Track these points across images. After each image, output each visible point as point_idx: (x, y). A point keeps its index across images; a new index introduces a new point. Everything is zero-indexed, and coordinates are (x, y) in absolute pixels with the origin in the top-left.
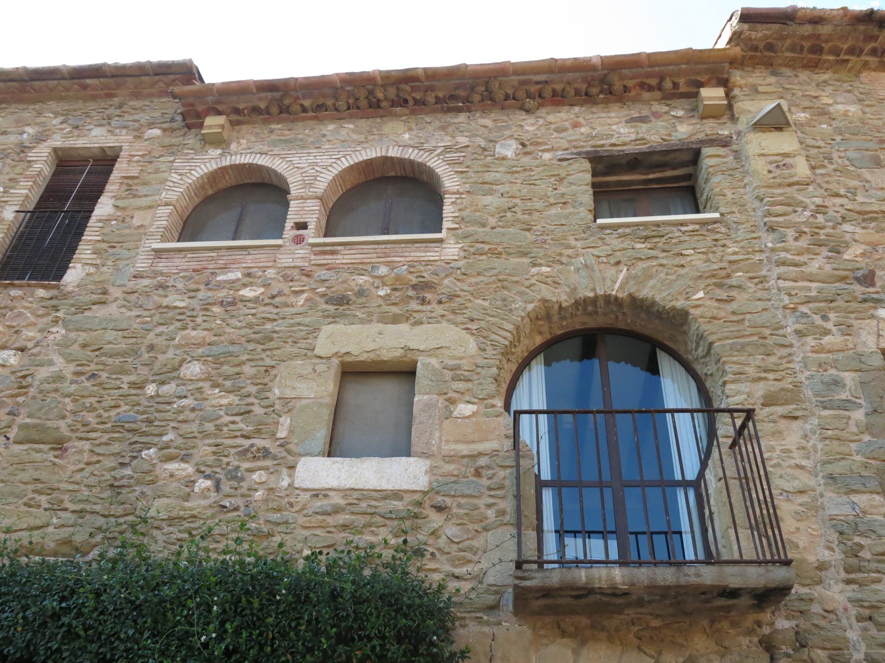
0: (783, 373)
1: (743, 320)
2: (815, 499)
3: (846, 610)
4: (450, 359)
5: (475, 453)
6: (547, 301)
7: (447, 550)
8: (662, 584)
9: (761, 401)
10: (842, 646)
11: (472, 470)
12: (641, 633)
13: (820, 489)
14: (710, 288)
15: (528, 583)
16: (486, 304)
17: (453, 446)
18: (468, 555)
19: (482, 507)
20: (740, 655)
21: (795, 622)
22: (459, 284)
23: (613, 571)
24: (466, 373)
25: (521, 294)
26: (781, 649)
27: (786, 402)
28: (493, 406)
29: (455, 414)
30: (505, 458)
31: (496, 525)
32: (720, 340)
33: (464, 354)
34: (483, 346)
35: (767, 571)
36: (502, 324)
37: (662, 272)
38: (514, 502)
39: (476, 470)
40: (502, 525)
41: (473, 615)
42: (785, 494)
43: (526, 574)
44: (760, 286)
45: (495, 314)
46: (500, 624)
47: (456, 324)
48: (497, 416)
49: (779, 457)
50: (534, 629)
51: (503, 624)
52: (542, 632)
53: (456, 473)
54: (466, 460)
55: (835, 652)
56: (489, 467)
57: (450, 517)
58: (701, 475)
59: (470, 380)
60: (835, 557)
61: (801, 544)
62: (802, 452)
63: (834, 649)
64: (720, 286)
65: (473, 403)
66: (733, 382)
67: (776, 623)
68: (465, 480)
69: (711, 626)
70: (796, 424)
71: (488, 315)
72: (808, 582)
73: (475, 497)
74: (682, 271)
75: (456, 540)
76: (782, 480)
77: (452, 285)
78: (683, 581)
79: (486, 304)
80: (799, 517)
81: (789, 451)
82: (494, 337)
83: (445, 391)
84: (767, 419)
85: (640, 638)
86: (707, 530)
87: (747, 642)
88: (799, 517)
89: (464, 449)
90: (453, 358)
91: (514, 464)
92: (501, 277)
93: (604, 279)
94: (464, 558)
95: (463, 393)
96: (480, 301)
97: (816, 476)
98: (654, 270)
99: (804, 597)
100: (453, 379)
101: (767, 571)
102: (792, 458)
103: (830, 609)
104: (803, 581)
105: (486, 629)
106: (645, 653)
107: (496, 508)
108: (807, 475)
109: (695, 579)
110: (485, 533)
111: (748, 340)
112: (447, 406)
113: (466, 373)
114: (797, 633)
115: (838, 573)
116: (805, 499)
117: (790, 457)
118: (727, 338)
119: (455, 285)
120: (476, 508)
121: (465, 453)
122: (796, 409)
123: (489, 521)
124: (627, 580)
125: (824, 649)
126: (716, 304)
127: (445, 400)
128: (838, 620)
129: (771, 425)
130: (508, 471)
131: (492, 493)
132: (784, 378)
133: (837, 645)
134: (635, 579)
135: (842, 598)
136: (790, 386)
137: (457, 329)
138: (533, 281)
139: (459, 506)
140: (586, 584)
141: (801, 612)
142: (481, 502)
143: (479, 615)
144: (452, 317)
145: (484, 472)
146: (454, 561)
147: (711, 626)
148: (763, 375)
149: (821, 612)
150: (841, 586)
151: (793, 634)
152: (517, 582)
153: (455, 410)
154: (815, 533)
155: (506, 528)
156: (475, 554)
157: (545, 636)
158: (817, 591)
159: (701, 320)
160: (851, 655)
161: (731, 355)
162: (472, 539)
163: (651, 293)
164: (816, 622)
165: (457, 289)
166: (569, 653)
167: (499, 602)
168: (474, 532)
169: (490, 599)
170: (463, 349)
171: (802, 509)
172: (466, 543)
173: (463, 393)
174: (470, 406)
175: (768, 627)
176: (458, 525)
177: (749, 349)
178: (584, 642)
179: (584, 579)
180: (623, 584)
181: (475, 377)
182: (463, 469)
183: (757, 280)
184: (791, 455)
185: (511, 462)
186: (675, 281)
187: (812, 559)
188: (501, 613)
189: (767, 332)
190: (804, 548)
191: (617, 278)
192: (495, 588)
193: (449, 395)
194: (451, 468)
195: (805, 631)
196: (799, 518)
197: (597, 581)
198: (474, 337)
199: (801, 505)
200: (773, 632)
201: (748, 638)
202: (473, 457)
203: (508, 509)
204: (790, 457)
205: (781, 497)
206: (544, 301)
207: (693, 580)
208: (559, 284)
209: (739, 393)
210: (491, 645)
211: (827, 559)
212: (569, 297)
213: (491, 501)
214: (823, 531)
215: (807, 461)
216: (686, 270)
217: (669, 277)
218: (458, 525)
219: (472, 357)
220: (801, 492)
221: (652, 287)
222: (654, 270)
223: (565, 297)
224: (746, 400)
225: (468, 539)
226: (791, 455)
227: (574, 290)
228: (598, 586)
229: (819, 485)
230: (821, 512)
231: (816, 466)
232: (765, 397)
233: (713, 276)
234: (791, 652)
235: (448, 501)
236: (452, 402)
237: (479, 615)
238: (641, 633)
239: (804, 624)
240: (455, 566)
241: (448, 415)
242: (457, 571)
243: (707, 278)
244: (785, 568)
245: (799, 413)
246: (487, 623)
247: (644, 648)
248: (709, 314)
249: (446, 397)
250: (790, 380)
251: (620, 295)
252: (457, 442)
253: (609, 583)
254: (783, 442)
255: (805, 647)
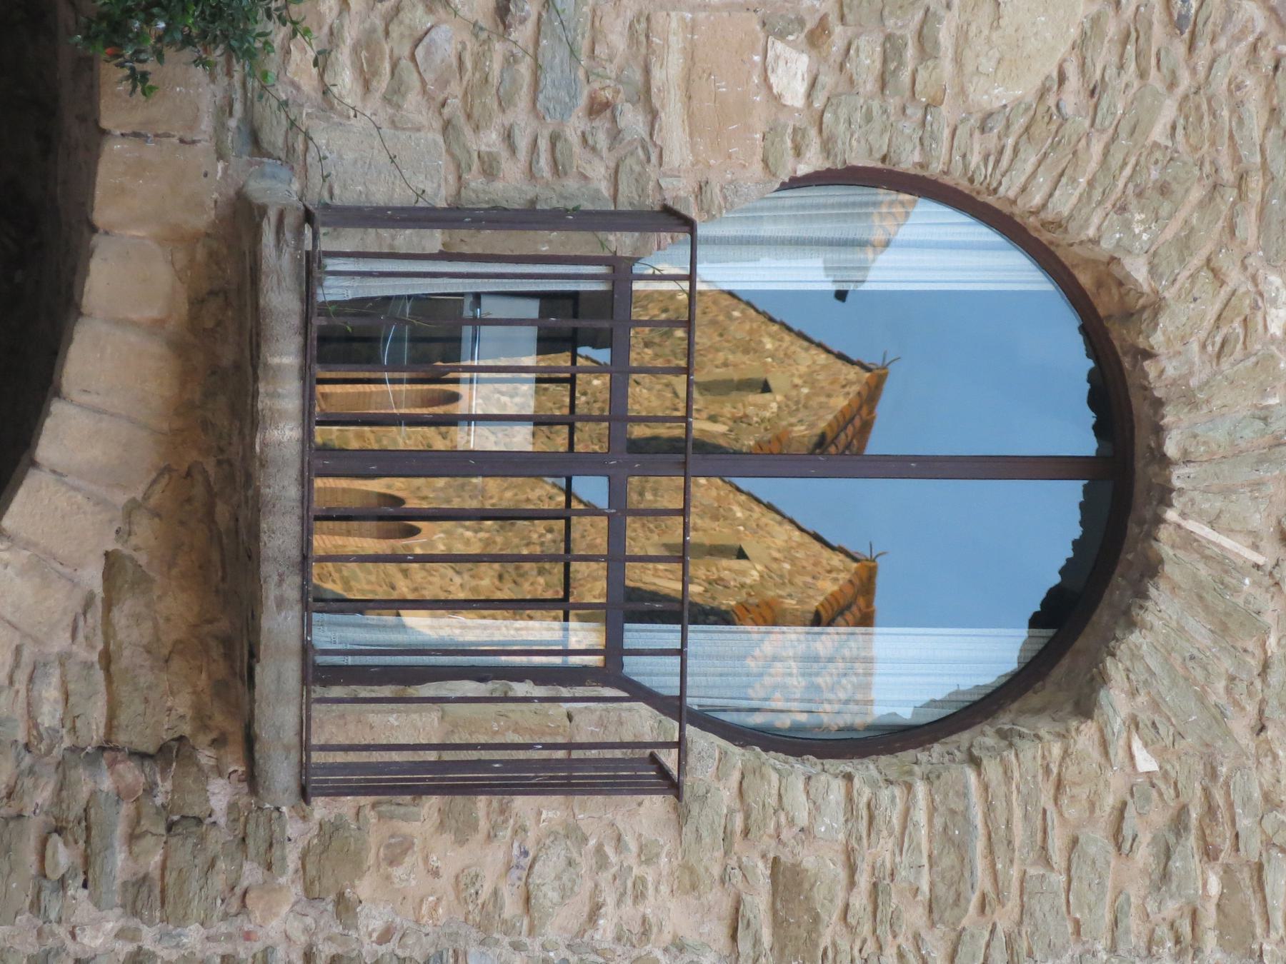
0: (866, 929)
1: (1047, 862)
2: (508, 928)
3: (248, 936)
4: (959, 28)
5: (656, 102)
6: (1156, 315)
7: (395, 30)
8: (264, 526)
9: (786, 858)
10: (169, 909)
11: (608, 94)
12: (199, 478)
13: (535, 945)
14: (1169, 793)
15: (268, 237)
16: (1158, 133)
17: (676, 42)
18: (383, 83)
19: (508, 119)
20: (149, 688)
21: (222, 821)
22: (1242, 48)
23: (292, 424)
24: (905, 76)
25: (1185, 244)
26: (164, 780)
27: (778, 923)
28: (798, 152)
29: (778, 47)
30: (640, 179)
31: (457, 152)
32: (986, 788)
33: (969, 68)
34: (998, 125)
35: (287, 749)
36: (1074, 180)
37: (1241, 664)
38: (517, 203)
39: (607, 105)
40: (459, 166)
41: (238, 95)
42: (526, 862)
43: (289, 236)
44: (1163, 931)
45: (1115, 161)
46: (221, 156)
47: (1082, 44)
48: (765, 161)
49: (624, 871)
50: (208, 235)
51: (220, 166)
52: (201, 254)
53: (601, 51)
54: (638, 76)
55: (157, 891)
56: (615, 135)
57: (484, 35)
58: (639, 693)
59: (883, 87)
60: (366, 940)
61: (398, 872)
62: (637, 928)
63: (163, 891)
64: (1179, 823)
65: (809, 95)
66: (850, 799)
67: (221, 782)
68: (581, 74)
69: (216, 637)
70: (719, 932)
71: (1114, 138)
72: (312, 871)
73: (534, 101)
74: (1240, 727)
75: (420, 52)
76: (562, 863)
77: (1233, 29)
78: (269, 570)
79: (1158, 133)
80: (465, 883)
81: (639, 897)
82: (1029, 160)
83: (850, 18)
84: (733, 862)
85: (189, 474)
86: (482, 680)
87: (181, 711)
88: (465, 883)
89: (668, 72)
90: (962, 37)
91: (624, 206)
92: (1255, 183)
93: (1226, 492)
94: (375, 73)
95: (842, 67)
96: (1169, 110)
97: (569, 946)
98: (1251, 645)
99: (276, 852)
100: (889, 38)
101: (287, 749)
102: (619, 902)
103: (248, 901)
104: (311, 859)
105: (206, 124)
106: (154, 482)
107: (504, 154)
108: (575, 926)
109: (272, 597)
110: (437, 125)
111: (980, 864)
112: (801, 22)
113: (905, 76)
114: (199, 821)
115: (329, 939)
116: (511, 907)
117: (623, 894)
118: (989, 808)
119: (1237, 39)
120: (504, 103)
121: (658, 75)
122: (757, 942)
123: (467, 131)
124: (272, 453)
125: (163, 868)
126: (1109, 802)
127: (823, 20)
128: (226, 916)
129: (716, 871)
130: (605, 188)
131: (543, 144)
132: (852, 930)
133: (170, 899)
134: (272, 470)
135: (272, 934)
136: (825, 941)
137: (1063, 49)
138: (1235, 277)
139: (511, 60)
140: (266, 364)
141: (244, 839)
142: (520, 115)
143: (238, 107)
144: (1112, 29)
145: (602, 124)
146: (368, 48)
147: (216, 637)
148: (864, 880)
149: (245, 884)
150: (302, 939)
151: (196, 811)
152: (273, 214)
153: (793, 45)
154: (425, 908)
155: (452, 179)
156: (387, 100)
157: (192, 260)
158: (289, 884)
159: (1056, 749)
160: (150, 923)
161: (933, 809)
162: (424, 91)
163: (1158, 624)
164: (221, 865)
165: (1222, 43)
166: (153, 313)
167: (270, 156)
168: (441, 98)
169: (275, 135)
170: (988, 66)
171: (485, 894)
172: (414, 79)
173: (842, 67)
174: (801, 88)
175: (212, 762)
176: (460, 58)
177: (949, 860)
178: (180, 349)
179: (275, 361)
180: (265, 445)
181: (893, 103)
182: (611, 70)
183: (1186, 928)
184: (629, 901)
185: (628, 198)
186: (1201, 699)
187: (364, 888)
188: (245, 158)
189: (1005, 918)
190: (388, 878)
191: (1229, 532)
192: (300, 147)
193: (838, 29)
194: (617, 39)
195: (202, 839)
196: (463, 880)
197: (271, 388)
198: (1031, 98)
199: (495, 893)
200: (200, 769)
201: (189, 714)
202: (645, 97)
203: (499, 185)
204: (623, 894)
205: (516, 851)
206: (1156, 306)
207: (271, 592)
208: (1219, 355)
209: (816, 808)
210: (168, 135)
211: (362, 921)
212: (1174, 382)
213: (523, 143)
214: (429, 929)
215: (610, 935)
216: (1245, 739)
217: (1221, 685)
218: (460, 58)
219: (962, 91)
220: (528, 900)
221: (1181, 630)
222: (1251, 645)
223: (1170, 372)
224: (791, 822)
225: (423, 82)
226: (629, 901)
227: (1190, 401)
228: (261, 390)
229: (543, 946)
230: (475, 934)
231: (596, 952)
232: (797, 872)
233: (1210, 810)
234: (159, 800)
235: (522, 34)
236: (817, 37)
237: (238, 107)
238: (199, 478)
239: (218, 839)
240: (355, 50)
241: (774, 28)
242: (343, 56)
243: (1206, 790)
244: (293, 785)
245: (745, 946)
246: (220, 127)
247: (164, 481)
248: (1071, 772)
249: (833, 18)
250: (844, 945)
251: (1164, 533)
252: (691, 56)
253: (267, 413)
254: (664, 889)
255: (169, 829)
